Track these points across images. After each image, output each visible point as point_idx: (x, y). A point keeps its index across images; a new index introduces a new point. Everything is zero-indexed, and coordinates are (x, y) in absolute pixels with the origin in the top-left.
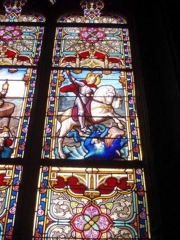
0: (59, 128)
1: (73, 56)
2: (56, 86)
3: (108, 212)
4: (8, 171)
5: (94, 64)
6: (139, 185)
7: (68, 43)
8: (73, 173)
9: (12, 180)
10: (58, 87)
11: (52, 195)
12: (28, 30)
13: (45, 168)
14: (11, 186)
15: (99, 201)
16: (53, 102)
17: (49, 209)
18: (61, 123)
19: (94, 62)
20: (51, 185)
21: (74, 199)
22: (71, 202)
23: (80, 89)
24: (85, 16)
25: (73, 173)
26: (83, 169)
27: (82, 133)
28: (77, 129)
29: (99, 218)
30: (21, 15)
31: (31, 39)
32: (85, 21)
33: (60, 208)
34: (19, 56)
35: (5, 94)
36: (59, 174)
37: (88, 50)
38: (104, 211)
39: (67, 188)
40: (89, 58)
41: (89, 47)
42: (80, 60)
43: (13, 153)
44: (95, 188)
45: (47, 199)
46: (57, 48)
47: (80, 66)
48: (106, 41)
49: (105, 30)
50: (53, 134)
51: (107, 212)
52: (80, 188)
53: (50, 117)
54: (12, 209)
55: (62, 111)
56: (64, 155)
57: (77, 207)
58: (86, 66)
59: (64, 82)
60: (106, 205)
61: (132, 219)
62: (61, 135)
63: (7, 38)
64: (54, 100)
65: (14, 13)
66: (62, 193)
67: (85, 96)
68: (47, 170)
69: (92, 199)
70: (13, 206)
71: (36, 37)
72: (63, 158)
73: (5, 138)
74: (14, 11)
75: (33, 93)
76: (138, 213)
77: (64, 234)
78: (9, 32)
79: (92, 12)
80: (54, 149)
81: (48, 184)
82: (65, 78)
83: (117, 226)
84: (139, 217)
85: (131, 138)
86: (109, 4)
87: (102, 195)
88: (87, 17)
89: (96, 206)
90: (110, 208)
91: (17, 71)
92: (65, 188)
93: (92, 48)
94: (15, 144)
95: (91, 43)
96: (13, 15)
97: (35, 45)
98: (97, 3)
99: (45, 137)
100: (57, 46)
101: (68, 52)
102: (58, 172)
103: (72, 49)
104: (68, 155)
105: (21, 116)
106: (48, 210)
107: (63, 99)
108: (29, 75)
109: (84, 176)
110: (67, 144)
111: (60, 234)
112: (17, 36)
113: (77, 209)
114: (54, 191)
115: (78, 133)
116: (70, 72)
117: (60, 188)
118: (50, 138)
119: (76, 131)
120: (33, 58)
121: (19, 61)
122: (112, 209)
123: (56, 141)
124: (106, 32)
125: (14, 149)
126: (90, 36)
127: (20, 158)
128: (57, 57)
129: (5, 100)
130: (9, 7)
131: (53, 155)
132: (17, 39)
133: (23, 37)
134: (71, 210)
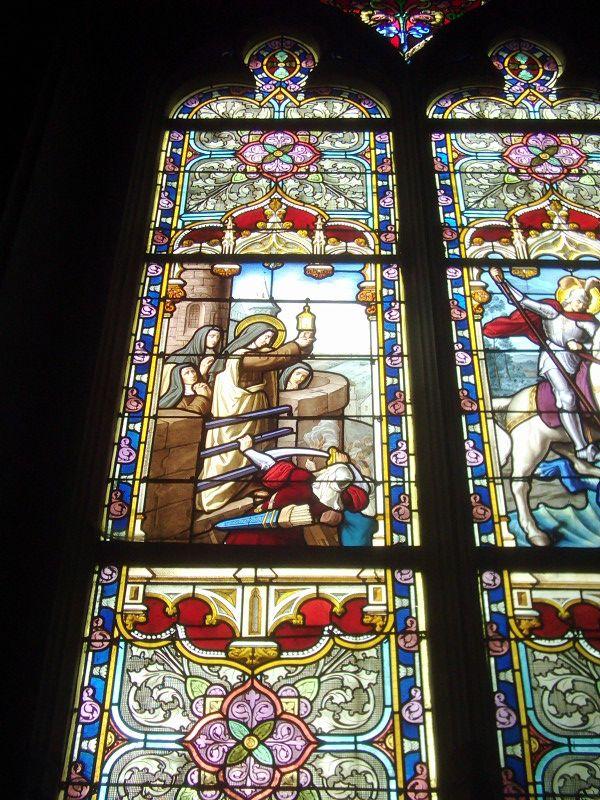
0: (507, 452)
1: (502, 223)
2: (467, 318)
3: (303, 709)
5: (570, 248)
6: (403, 615)
7: (473, 181)
8: (194, 585)
9: (391, 617)
10: (475, 320)
11: (530, 662)
12: (338, 144)
14: (392, 637)
15: (274, 675)
16: (468, 370)
18: (509, 433)
19: (571, 242)
20: (521, 631)
21: (197, 670)
23: (547, 327)
24: (511, 98)
26: (227, 573)
27: (585, 464)
28: (564, 452)
29: (275, 728)
30: (306, 98)
31: (356, 173)
32: (511, 112)
33: (567, 703)
34: (329, 224)
35: (310, 347)
36: (537, 594)
37: (262, 205)
38: (290, 705)
39: (575, 640)
40: (551, 229)
41: (544, 195)
42: (526, 235)
43: (376, 530)
44: (263, 634)
45: (517, 674)
47: (529, 256)
48: (591, 175)
49: (582, 141)
50: (493, 470)
51: (299, 710)
52: (218, 636)
53: (473, 418)
54: (408, 709)
55: (505, 397)
56: (540, 534)
57: (299, 697)
58: (549, 255)
59: (492, 304)
60: (296, 686)
62: (518, 472)
63: (277, 170)
64: (472, 363)
65: (283, 90)
66: (563, 652)
67: (567, 348)
68: (498, 582)
69: (253, 667)
71: (368, 167)
72: (540, 543)
73: (340, 483)
74: (280, 84)
76: (396, 708)
77: (164, 777)
78: (279, 149)
79: (527, 86)
81: (509, 628)
82: (491, 294)
83: (330, 752)
84: (402, 719)
86: (339, 57)
88: (264, 98)
89: (266, 691)
90: (308, 696)
91: (332, 272)
92: (569, 639)
93: (276, 195)
94: (378, 505)
95: (272, 180)
96: (281, 97)
97: (185, 190)
98: (538, 55)
100: (167, 194)
101: (481, 210)
103: (490, 202)
104: (553, 535)
105: (377, 413)
106: (527, 709)
107: (499, 359)
108: (373, 284)
110: (543, 499)
111: (584, 785)
112: (310, 163)
113: (295, 697)
114: (534, 650)
115: (572, 464)
116: (503, 272)
117: (553, 639)
118: (484, 482)
119: (563, 457)
120: (373, 230)
121: (332, 240)
122: (316, 697)
123: (508, 490)
124: (584, 148)
125: (379, 517)
126: (538, 161)
127: (403, 546)
128: (449, 227)
129: (315, 365)
130: (264, 71)
131: (506, 533)
132: (308, 172)
133: (327, 164)
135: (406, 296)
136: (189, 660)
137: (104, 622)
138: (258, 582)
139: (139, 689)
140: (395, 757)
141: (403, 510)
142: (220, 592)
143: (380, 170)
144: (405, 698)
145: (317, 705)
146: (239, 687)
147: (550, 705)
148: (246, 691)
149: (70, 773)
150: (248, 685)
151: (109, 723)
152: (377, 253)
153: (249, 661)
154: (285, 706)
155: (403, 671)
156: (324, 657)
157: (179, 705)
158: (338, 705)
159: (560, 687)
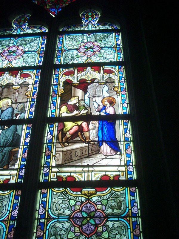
4: (12, 176)
8: (71, 173)
11: (52, 195)
13: (43, 191)
15: (95, 199)
17: (49, 207)
24: (84, 26)
25: (71, 173)
30: (97, 26)
36: (59, 174)
46: (49, 136)
54: (14, 212)
61: (125, 221)
69: (89, 196)
70: (16, 209)
75: (37, 92)
76: (130, 208)
77: (65, 229)
80: (55, 155)
84: (11, 214)
87: (98, 193)
89: (93, 203)
90: (105, 204)
99: (46, 143)
108: (118, 86)
109: (81, 175)
121: (22, 78)
134: (70, 208)
136: (70, 195)
137: (41, 227)
138: (88, 171)
140: (7, 226)
146: (85, 202)
147: (55, 207)
154: (99, 228)
155: (132, 198)
157: (67, 208)
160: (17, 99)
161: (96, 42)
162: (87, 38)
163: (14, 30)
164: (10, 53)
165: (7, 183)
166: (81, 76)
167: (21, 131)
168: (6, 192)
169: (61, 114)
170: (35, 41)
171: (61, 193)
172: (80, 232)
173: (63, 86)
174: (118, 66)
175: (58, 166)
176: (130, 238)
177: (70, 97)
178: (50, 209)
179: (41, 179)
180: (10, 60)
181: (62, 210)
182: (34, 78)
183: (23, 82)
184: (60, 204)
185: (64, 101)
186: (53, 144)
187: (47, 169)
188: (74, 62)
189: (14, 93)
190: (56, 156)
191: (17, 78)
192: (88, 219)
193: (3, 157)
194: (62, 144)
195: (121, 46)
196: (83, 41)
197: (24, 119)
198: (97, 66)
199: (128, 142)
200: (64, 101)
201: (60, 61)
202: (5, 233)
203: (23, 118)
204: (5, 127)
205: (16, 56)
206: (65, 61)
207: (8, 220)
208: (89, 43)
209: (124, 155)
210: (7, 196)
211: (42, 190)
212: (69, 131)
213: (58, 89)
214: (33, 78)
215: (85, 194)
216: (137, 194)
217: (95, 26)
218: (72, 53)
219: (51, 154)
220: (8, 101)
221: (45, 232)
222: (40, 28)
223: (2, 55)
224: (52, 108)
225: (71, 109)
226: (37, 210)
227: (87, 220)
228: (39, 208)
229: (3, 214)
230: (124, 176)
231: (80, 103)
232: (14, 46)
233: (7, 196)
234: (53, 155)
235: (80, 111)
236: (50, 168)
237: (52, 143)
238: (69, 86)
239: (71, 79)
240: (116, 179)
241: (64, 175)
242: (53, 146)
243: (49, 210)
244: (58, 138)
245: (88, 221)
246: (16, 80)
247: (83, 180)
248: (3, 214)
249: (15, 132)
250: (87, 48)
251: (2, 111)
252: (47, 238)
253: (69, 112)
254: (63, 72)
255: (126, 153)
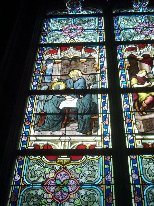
8: (82, 141)
11: (142, 161)
15: (69, 167)
22: (45, 169)
24: (135, 9)
30: (81, 11)
36: (36, 143)
43: (99, 129)
54: (107, 177)
60: (75, 170)
66: (37, 160)
76: (104, 176)
78: (73, 31)
80: (135, 123)
84: (105, 179)
85: (102, 113)
87: (72, 162)
102: (35, 141)
121: (87, 52)
127: (107, 148)
135: (107, 56)
136: (45, 163)
139: (32, 171)
140: (103, 190)
141: (110, 198)
142: (54, 143)
143: (101, 50)
144: (107, 174)
145: (81, 175)
147: (148, 173)
148: (62, 172)
149: (26, 120)
150: (62, 170)
151: (23, 180)
152: (103, 147)
153: (62, 163)
156: (83, 162)
158: (87, 175)
159: (150, 168)
160: (86, 71)
161: (150, 23)
162: (141, 19)
163: (69, 11)
164: (71, 30)
165: (94, 148)
166: (144, 52)
167: (96, 99)
168: (94, 157)
169: (133, 85)
170: (92, 21)
171: (151, 160)
172: (53, 198)
173: (128, 61)
174: (99, 46)
175: (140, 134)
176: (102, 205)
177: (138, 71)
178: (25, 176)
179: (20, 148)
180: (72, 37)
181: (37, 178)
182: (99, 53)
183: (89, 56)
184: (152, 170)
185: (133, 73)
186: (131, 113)
187: (131, 137)
188: (134, 40)
189: (83, 66)
190: (137, 123)
191: (82, 52)
192: (62, 187)
193: (84, 124)
194: (140, 113)
195: (103, 27)
196: (137, 21)
197: (97, 89)
198: (78, 46)
199: (106, 115)
200: (133, 73)
201: (119, 38)
202: (102, 197)
203: (96, 88)
204: (80, 95)
205: (77, 33)
206: (125, 39)
207: (103, 185)
208: (73, 26)
209: (101, 126)
210: (96, 161)
211: (131, 156)
212: (144, 101)
213: (124, 63)
214: (98, 53)
215: (60, 163)
216: (111, 163)
217: (146, 9)
218: (129, 32)
219: (131, 122)
220: (78, 72)
221: (143, 197)
222: (94, 11)
223: (63, 32)
224: (122, 79)
225: (142, 80)
226: (131, 176)
227: (60, 187)
228: (132, 174)
229: (96, 178)
230: (140, 144)
231: (149, 75)
232: (72, 25)
233: (96, 161)
234: (134, 124)
235: (150, 83)
236: (134, 135)
237: (130, 111)
238: (133, 61)
239: (134, 54)
240: (92, 148)
241: (41, 144)
242: (131, 115)
243: (142, 176)
244: (135, 108)
245: (62, 189)
246: (81, 54)
247: (59, 148)
248: (96, 178)
249: (91, 100)
250: (70, 29)
251: (74, 82)
252: (19, 205)
253: (140, 84)
254: (125, 49)
255: (103, 124)
